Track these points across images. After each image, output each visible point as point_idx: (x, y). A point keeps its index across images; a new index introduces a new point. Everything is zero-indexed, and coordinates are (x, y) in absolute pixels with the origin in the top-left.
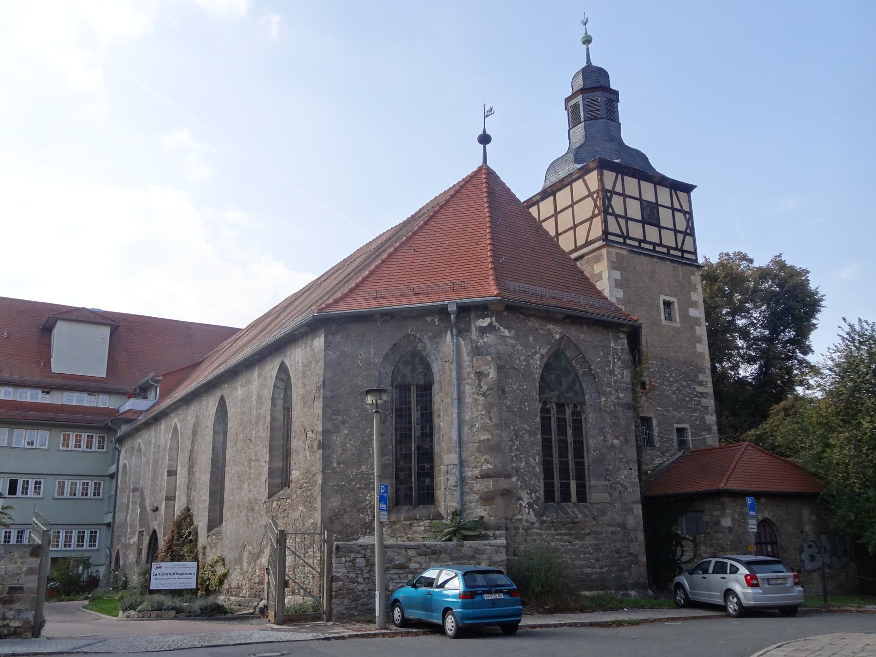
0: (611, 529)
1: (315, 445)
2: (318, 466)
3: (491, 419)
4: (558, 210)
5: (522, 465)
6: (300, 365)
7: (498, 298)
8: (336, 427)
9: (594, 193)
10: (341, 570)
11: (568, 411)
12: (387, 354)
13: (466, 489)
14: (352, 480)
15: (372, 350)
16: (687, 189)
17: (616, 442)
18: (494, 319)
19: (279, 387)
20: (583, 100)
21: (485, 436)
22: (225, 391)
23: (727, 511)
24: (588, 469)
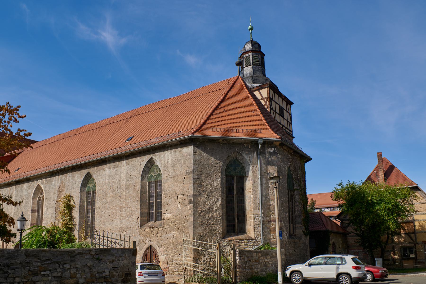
1: (187, 202)
2: (191, 212)
6: (170, 160)
9: (265, 98)
18: (276, 149)
19: (146, 171)
20: (252, 55)
22: (92, 170)
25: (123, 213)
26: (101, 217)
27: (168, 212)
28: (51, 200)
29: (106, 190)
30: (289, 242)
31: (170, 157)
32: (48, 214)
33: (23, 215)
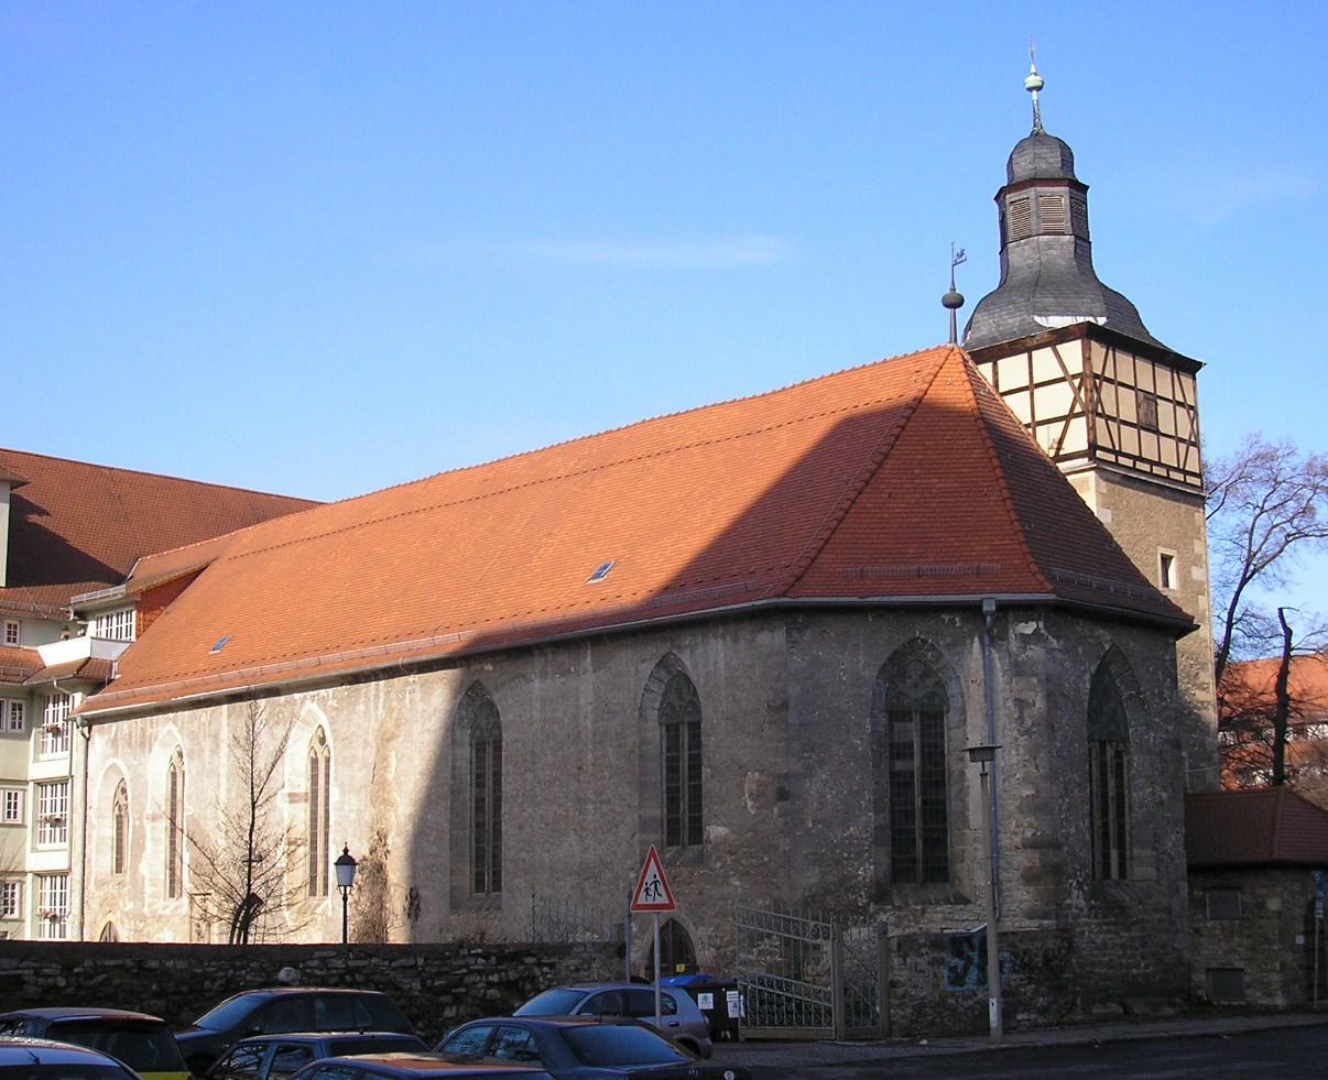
0: (1158, 916)
3: (1037, 767)
4: (1063, 423)
5: (1073, 830)
6: (722, 665)
7: (1053, 597)
8: (809, 768)
9: (1074, 377)
10: (903, 973)
11: (1110, 752)
12: (885, 665)
13: (1003, 863)
14: (836, 846)
15: (861, 657)
16: (1188, 367)
17: (1164, 795)
18: (1041, 625)
21: (1028, 792)
23: (623, 762)
24: (1130, 833)
25: (589, 817)
26: (521, 827)
27: (719, 822)
28: (356, 766)
29: (534, 744)
30: (1091, 908)
31: (722, 656)
32: (346, 808)
33: (346, 851)
